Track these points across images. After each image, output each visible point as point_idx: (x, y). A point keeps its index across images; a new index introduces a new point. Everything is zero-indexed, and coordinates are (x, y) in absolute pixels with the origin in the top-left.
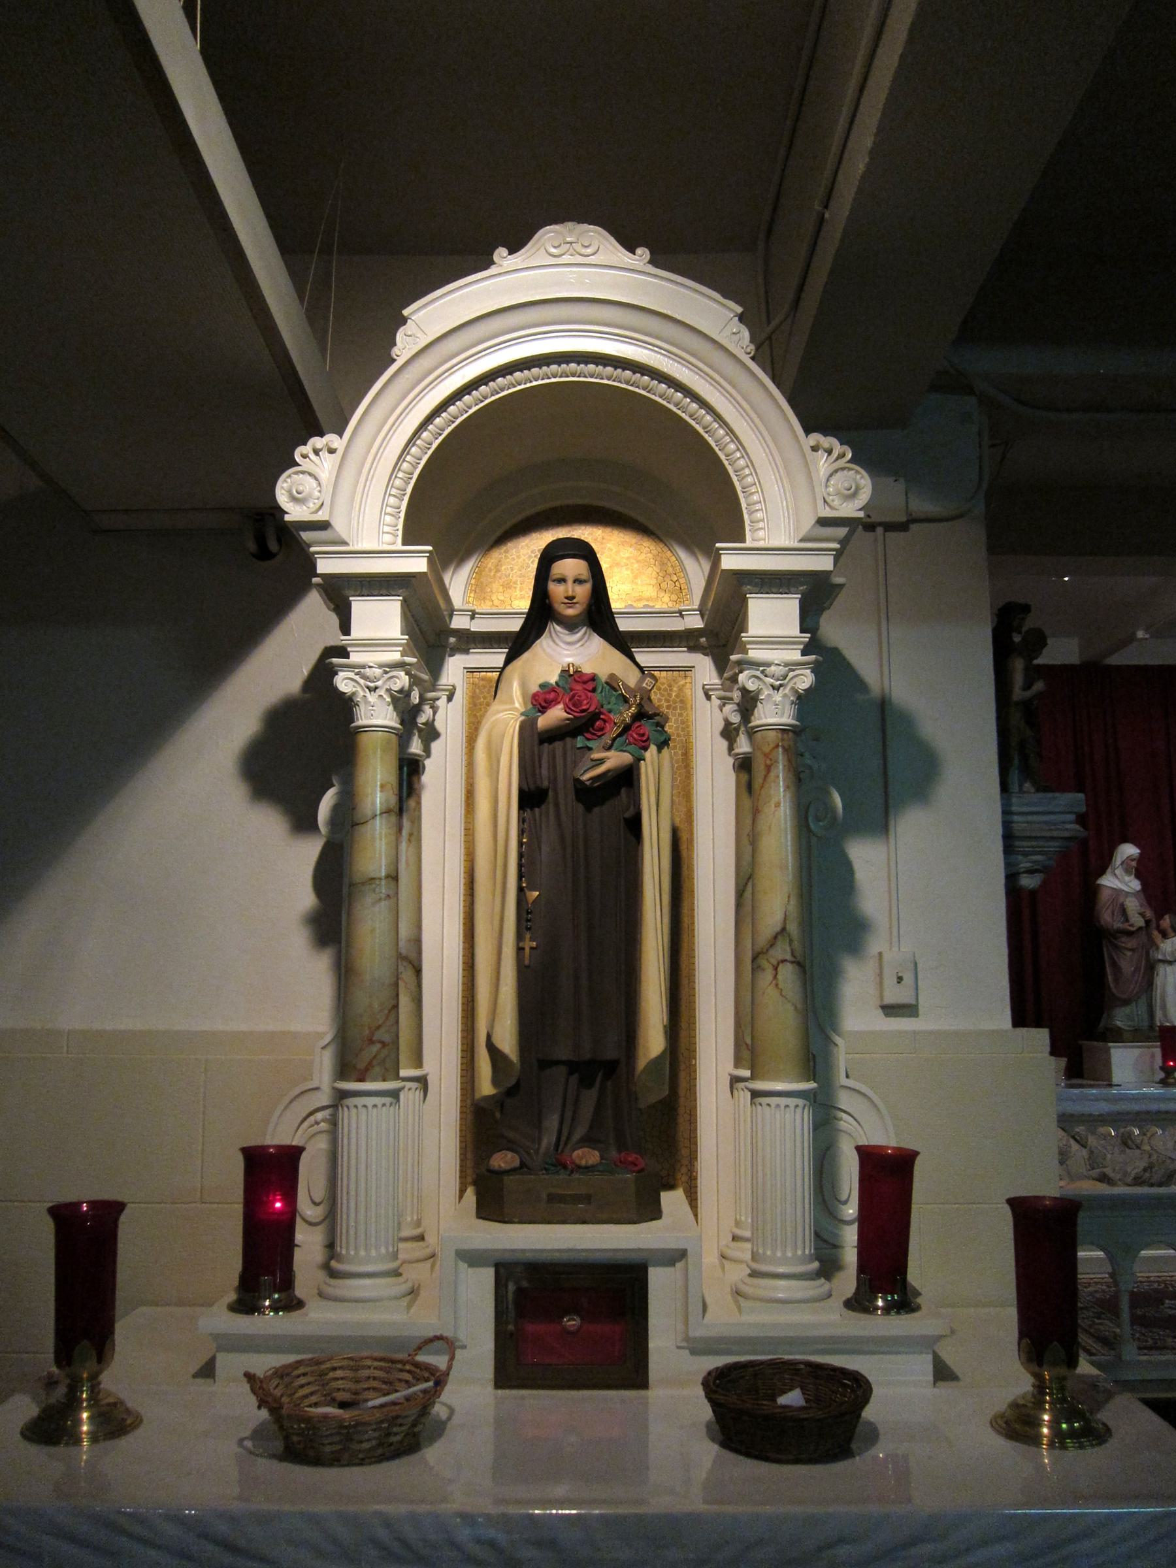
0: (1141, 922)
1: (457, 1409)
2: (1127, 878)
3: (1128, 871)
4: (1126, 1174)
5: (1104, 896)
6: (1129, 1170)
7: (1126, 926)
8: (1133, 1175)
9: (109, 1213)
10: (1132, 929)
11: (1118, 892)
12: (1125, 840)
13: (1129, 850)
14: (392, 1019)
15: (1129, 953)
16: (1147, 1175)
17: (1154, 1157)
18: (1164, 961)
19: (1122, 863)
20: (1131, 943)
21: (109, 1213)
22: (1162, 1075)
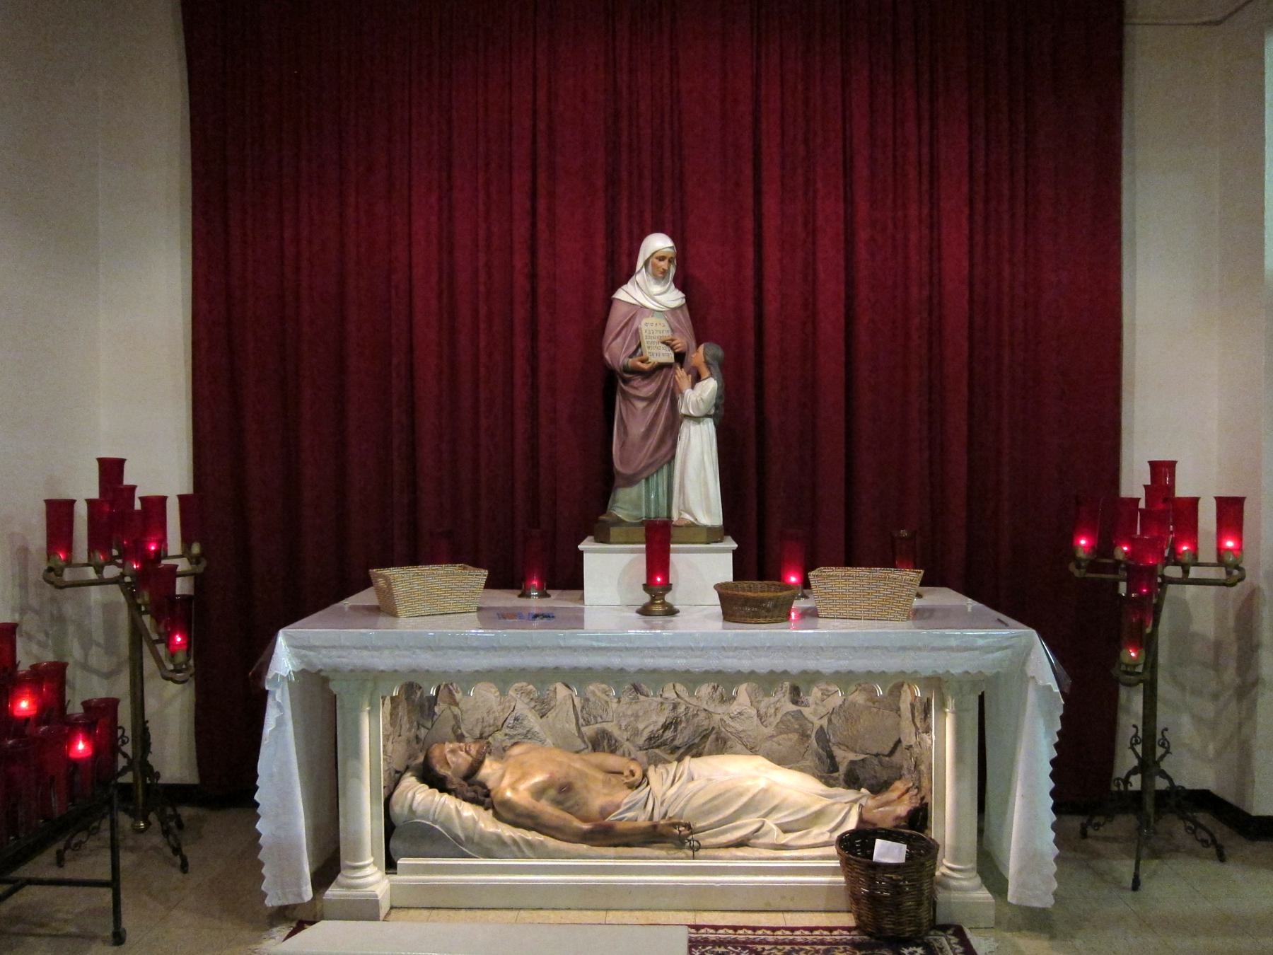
0: (667, 356)
1: (1247, 579)
2: (656, 289)
3: (660, 276)
4: (636, 733)
5: (617, 317)
6: (641, 726)
7: (635, 362)
8: (646, 735)
9: (1171, 465)
10: (645, 366)
11: (639, 310)
12: (658, 228)
13: (658, 243)
14: (669, 443)
15: (640, 405)
16: (669, 734)
17: (682, 709)
18: (690, 417)
19: (646, 264)
20: (647, 389)
21: (1171, 465)
22: (645, 598)
